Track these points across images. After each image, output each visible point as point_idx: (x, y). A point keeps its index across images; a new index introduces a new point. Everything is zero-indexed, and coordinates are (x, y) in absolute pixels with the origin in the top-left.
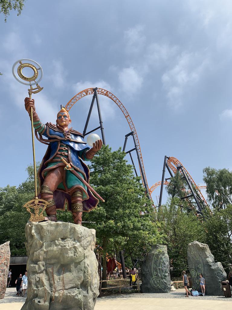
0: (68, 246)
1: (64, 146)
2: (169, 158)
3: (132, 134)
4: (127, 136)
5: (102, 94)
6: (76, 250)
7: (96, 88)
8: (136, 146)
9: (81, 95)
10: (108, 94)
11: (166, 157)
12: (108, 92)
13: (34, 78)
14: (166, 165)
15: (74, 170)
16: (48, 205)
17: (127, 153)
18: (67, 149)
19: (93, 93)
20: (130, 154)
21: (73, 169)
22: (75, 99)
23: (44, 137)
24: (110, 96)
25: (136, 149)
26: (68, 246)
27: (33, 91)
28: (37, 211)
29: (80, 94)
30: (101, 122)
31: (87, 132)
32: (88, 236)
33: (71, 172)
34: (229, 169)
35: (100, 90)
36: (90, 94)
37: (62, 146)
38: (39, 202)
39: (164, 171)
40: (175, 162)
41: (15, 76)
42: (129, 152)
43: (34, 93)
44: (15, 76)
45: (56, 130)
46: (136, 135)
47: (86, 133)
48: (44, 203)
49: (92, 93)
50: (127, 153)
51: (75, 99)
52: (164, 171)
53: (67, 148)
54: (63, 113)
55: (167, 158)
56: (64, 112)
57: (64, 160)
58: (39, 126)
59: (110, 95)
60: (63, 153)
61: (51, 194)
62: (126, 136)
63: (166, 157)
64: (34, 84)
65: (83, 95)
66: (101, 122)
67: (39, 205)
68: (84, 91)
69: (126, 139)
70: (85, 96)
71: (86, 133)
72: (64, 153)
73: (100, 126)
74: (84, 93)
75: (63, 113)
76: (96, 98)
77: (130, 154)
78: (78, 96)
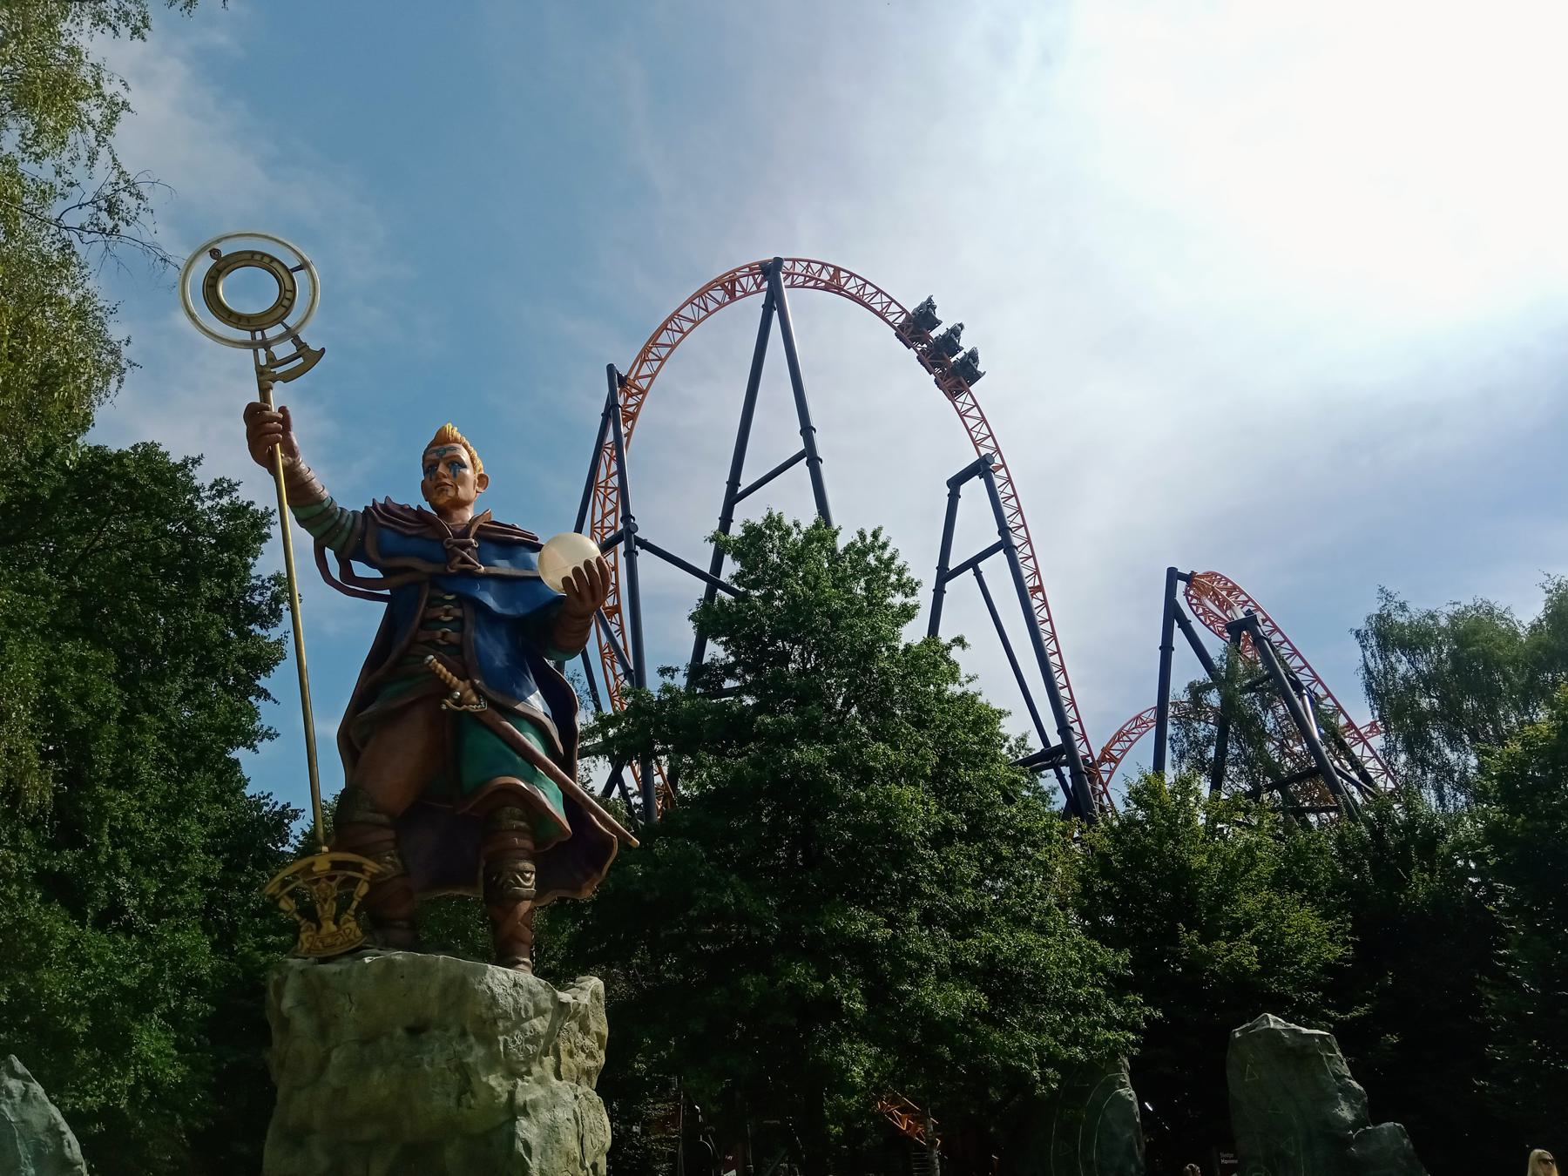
0: (432, 1064)
1: (449, 602)
2: (1190, 579)
3: (982, 468)
4: (955, 483)
5: (812, 284)
6: (469, 1082)
7: (778, 262)
8: (1004, 530)
9: (702, 305)
10: (843, 281)
11: (1173, 575)
12: (842, 274)
13: (282, 310)
14: (1172, 613)
15: (492, 711)
16: (373, 876)
17: (961, 569)
18: (458, 612)
19: (765, 285)
20: (978, 574)
21: (484, 706)
22: (675, 327)
23: (360, 569)
24: (854, 291)
25: (1005, 545)
26: (432, 1064)
27: (279, 370)
28: (326, 907)
29: (696, 301)
30: (807, 430)
31: (745, 482)
32: (531, 1013)
33: (475, 717)
34: (980, 694)
35: (799, 269)
36: (746, 293)
37: (435, 603)
38: (336, 865)
39: (1167, 648)
40: (1225, 600)
41: (192, 316)
42: (973, 563)
43: (288, 377)
44: (192, 316)
45: (408, 532)
46: (1002, 472)
47: (740, 490)
48: (359, 868)
49: (758, 286)
50: (961, 569)
51: (675, 327)
52: (1167, 648)
53: (461, 607)
54: (445, 450)
55: (1183, 577)
56: (446, 446)
57: (440, 666)
58: (328, 524)
59: (852, 286)
60: (439, 634)
61: (380, 826)
62: (949, 483)
63: (1173, 575)
64: (281, 338)
65: (712, 306)
66: (807, 430)
67: (332, 878)
68: (719, 283)
69: (954, 498)
70: (721, 305)
71: (740, 490)
72: (445, 634)
73: (801, 446)
74: (719, 294)
75: (450, 449)
76: (776, 313)
77: (978, 574)
78: (686, 312)
